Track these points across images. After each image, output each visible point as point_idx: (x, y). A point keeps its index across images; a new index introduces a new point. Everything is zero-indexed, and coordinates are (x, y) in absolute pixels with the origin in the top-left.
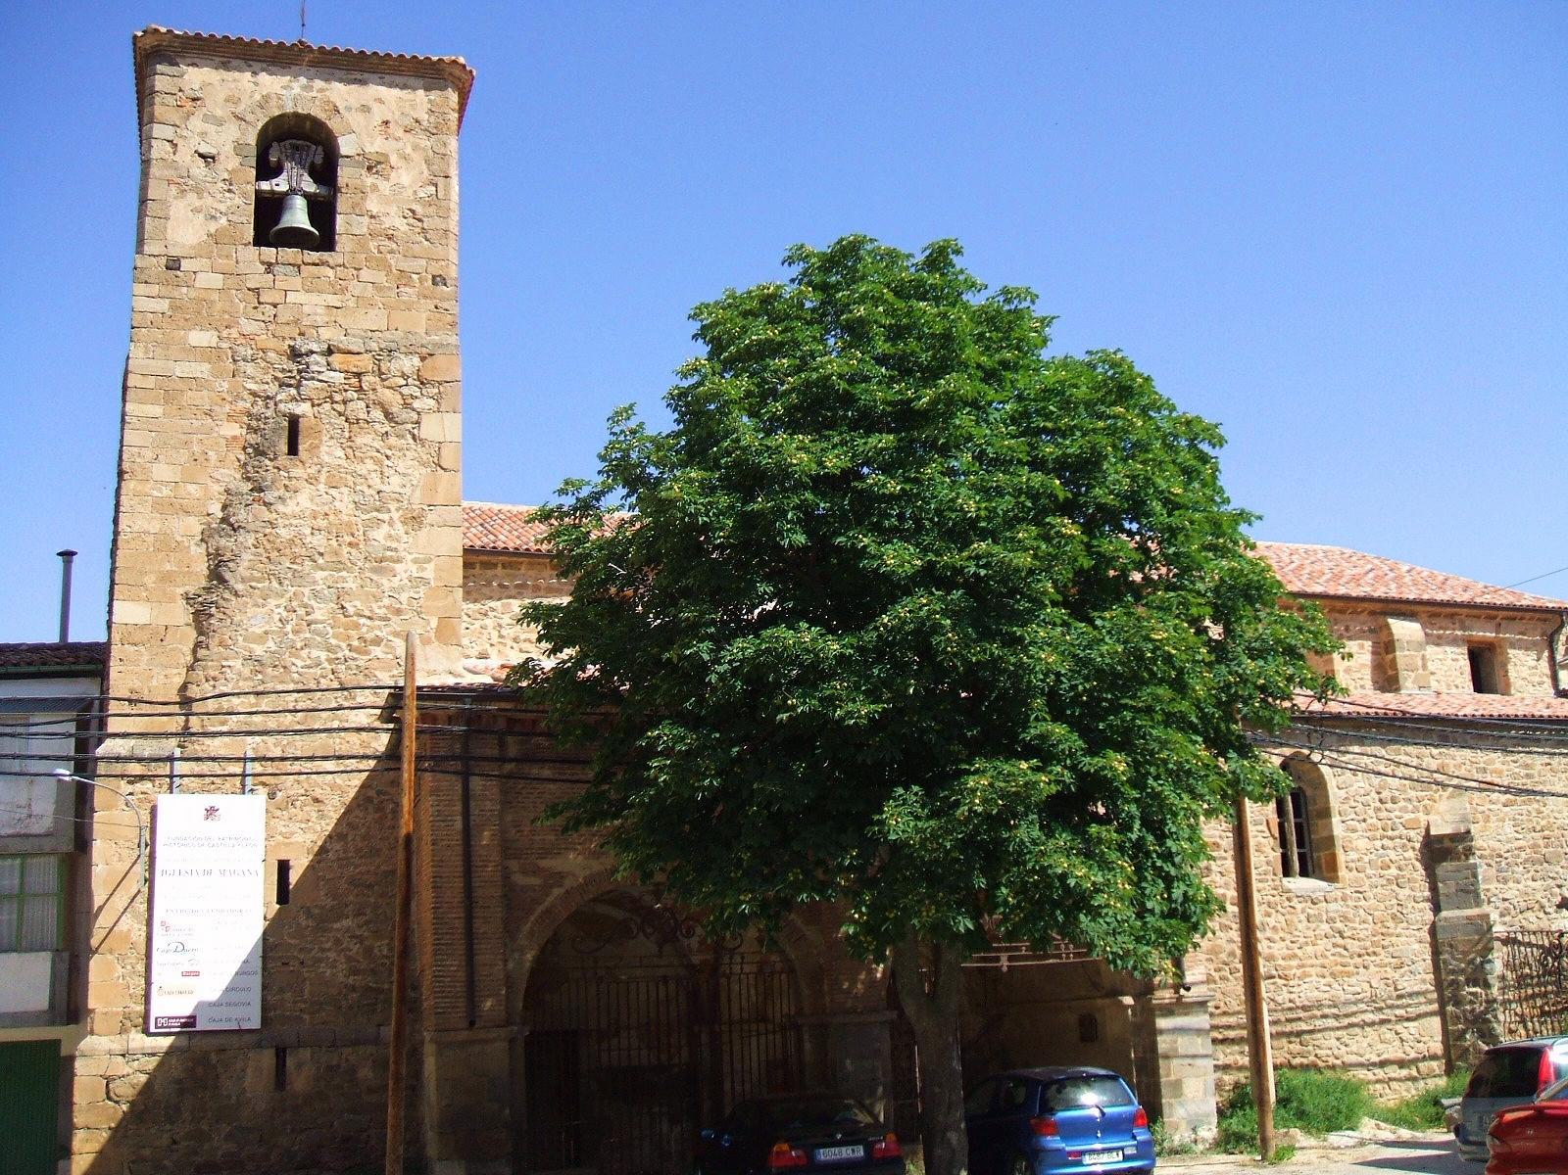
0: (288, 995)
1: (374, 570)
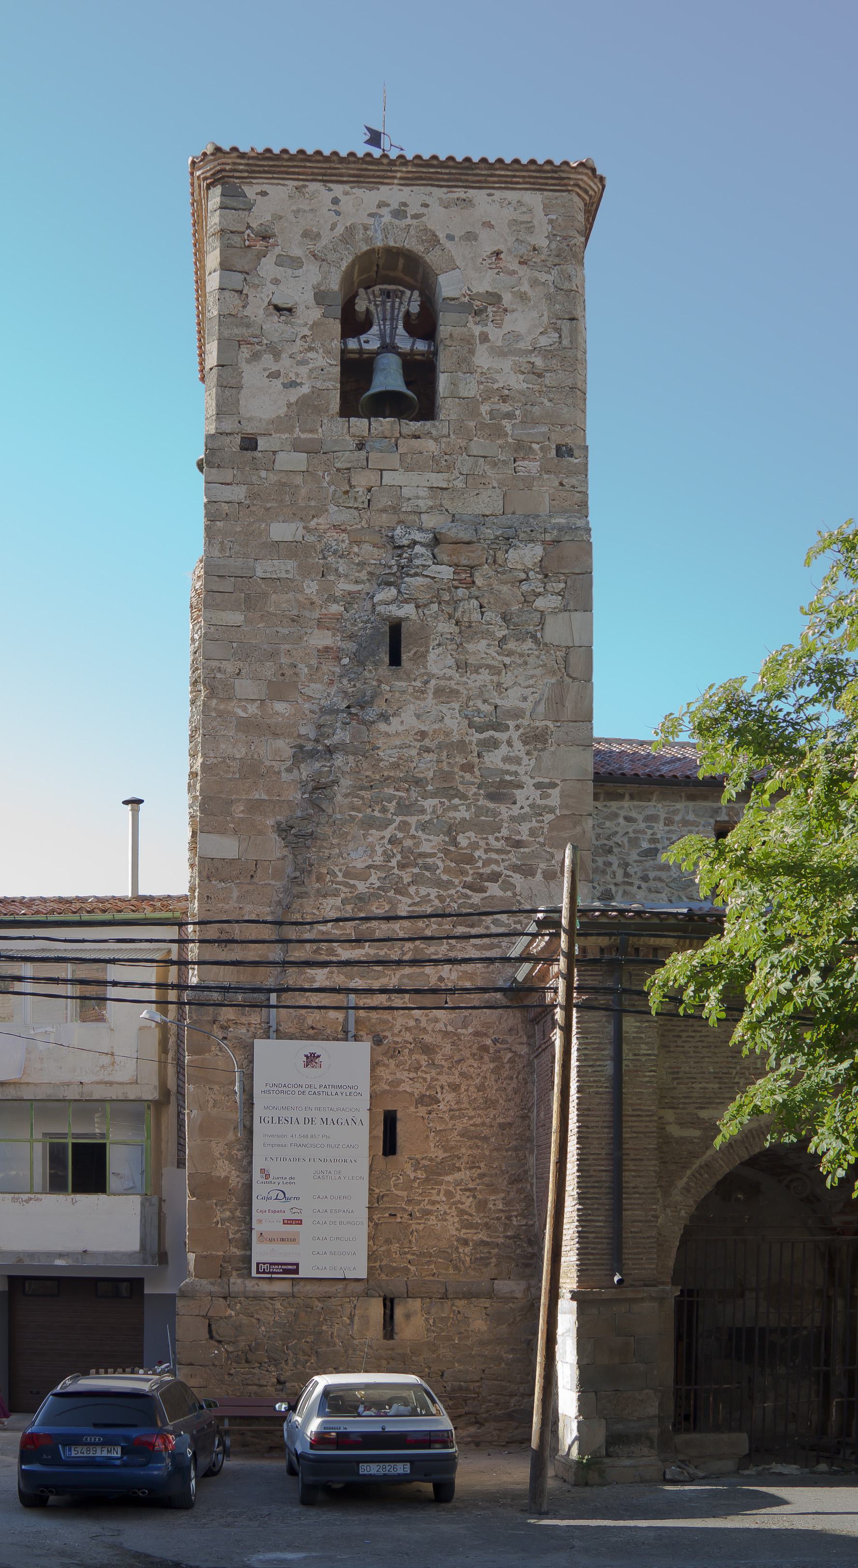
0: (395, 1246)
1: (491, 797)
